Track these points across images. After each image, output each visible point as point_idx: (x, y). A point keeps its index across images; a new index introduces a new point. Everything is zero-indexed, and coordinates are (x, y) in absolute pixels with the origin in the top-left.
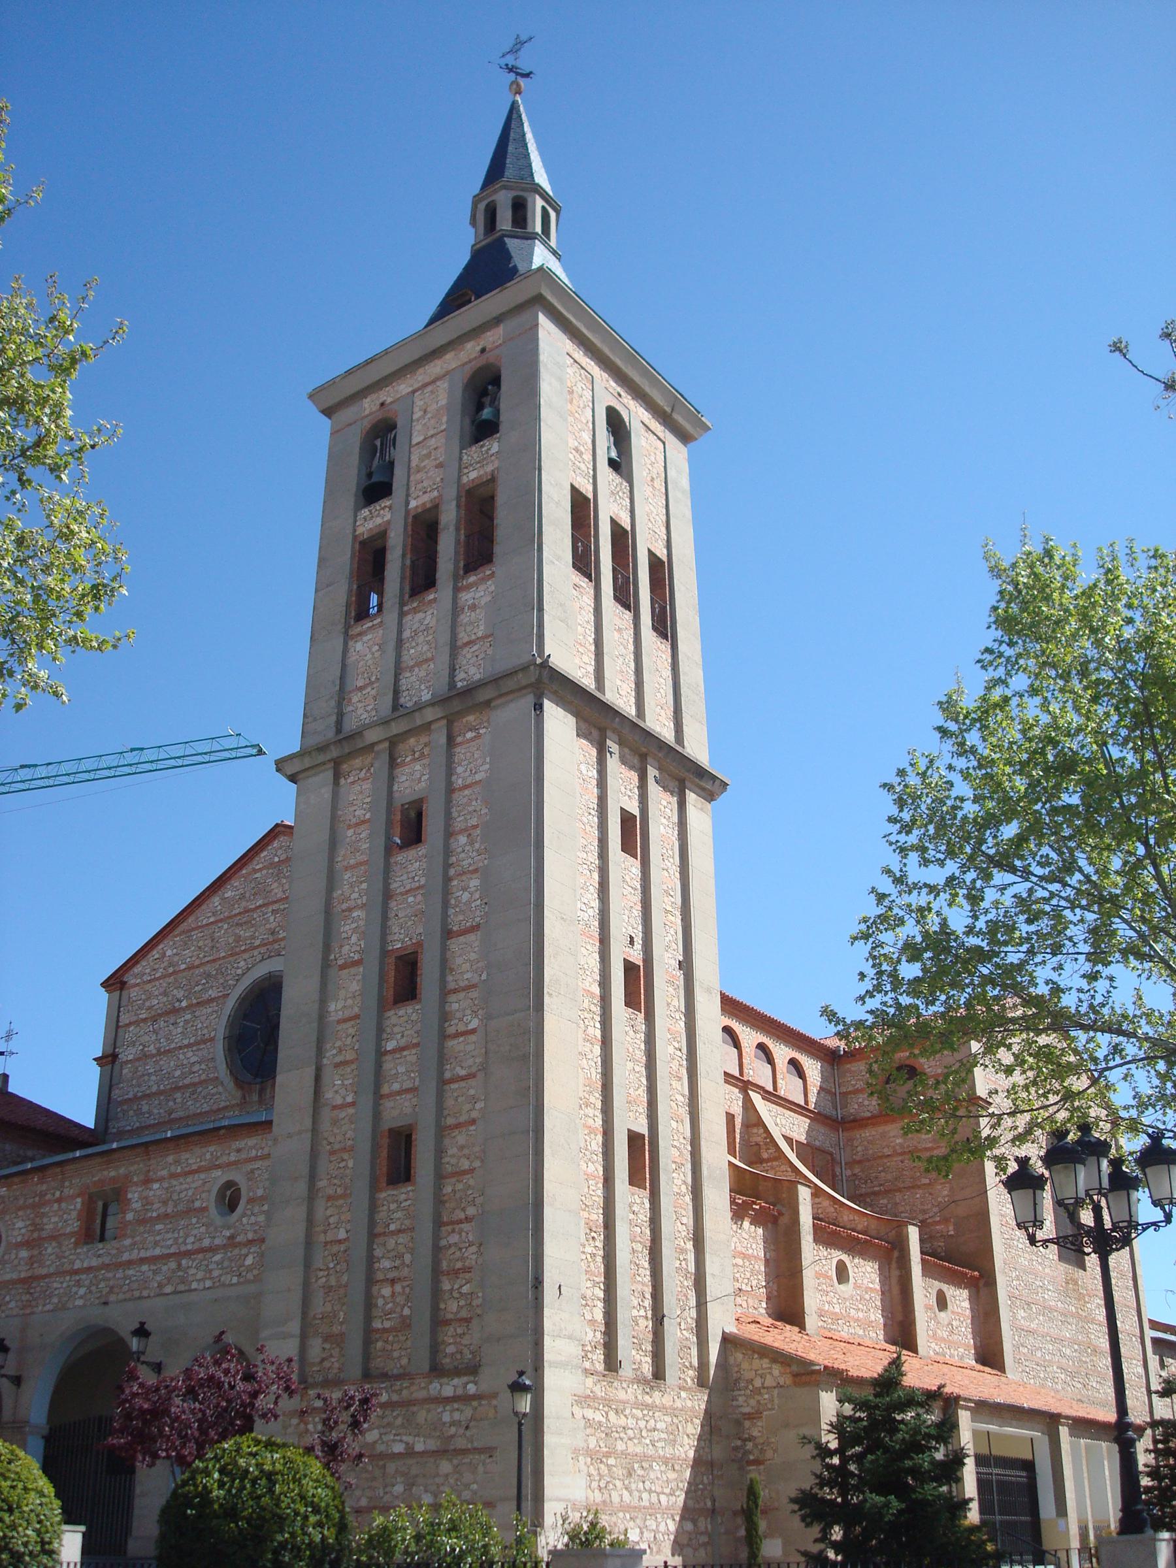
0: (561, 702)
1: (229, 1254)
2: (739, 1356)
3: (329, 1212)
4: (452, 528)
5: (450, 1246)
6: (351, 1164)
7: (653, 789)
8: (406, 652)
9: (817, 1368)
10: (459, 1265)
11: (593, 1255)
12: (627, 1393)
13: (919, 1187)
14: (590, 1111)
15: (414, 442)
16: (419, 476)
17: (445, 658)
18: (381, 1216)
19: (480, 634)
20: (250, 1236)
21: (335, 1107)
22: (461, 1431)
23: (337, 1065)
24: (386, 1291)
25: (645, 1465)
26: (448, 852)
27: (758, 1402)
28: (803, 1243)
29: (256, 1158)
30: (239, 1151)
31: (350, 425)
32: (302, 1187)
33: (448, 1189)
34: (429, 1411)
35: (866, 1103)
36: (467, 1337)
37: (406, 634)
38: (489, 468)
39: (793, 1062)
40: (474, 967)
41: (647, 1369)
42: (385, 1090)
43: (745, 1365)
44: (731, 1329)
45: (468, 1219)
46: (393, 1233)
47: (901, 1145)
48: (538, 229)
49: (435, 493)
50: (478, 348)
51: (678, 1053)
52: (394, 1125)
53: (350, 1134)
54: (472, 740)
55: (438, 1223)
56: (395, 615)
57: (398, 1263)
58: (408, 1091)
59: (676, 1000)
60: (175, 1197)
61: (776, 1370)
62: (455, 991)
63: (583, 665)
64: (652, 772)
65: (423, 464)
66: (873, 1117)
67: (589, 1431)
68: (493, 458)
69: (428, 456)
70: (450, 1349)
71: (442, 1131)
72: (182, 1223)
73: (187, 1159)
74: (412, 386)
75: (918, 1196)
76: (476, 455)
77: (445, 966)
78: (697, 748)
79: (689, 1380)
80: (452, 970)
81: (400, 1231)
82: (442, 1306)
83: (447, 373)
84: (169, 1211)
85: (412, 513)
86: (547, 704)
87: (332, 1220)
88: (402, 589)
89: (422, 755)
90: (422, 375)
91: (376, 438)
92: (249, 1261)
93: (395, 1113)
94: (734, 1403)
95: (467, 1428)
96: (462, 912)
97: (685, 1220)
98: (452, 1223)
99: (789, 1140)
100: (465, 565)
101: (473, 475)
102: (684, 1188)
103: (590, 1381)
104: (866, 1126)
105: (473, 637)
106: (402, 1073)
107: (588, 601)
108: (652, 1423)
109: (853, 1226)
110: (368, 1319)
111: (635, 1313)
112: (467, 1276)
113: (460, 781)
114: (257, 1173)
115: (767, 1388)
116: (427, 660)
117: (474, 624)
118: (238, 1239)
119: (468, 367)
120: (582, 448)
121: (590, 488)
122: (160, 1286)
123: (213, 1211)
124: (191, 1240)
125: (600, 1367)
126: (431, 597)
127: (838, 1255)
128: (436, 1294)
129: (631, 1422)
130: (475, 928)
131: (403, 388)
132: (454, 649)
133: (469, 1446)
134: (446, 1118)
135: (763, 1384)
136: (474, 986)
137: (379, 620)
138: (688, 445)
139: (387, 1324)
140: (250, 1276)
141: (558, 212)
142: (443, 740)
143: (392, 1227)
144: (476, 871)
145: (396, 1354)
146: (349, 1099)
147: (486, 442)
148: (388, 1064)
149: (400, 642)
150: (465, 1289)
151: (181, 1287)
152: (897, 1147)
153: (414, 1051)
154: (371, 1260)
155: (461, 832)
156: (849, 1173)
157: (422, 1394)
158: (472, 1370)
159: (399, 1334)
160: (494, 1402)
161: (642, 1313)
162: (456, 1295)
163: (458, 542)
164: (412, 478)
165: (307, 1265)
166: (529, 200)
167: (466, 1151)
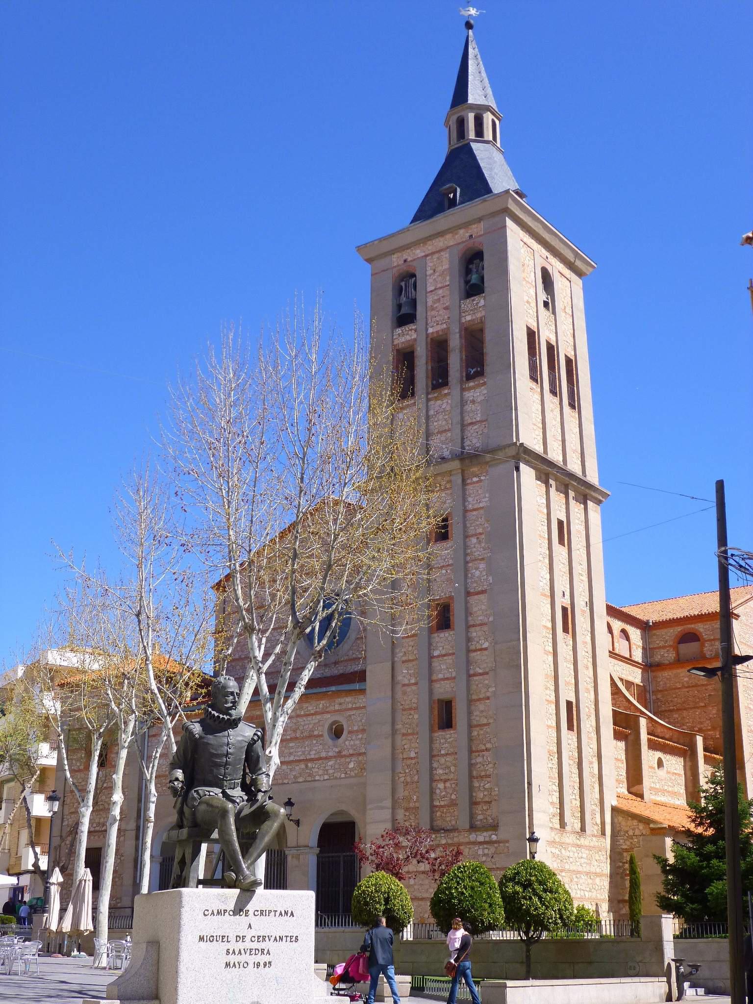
0: (527, 463)
1: (338, 761)
2: (620, 819)
3: (403, 743)
4: (457, 351)
5: (477, 764)
6: (416, 716)
7: (572, 502)
8: (432, 424)
9: (665, 826)
10: (483, 774)
11: (552, 768)
12: (570, 839)
13: (698, 708)
14: (548, 692)
15: (429, 289)
16: (433, 313)
17: (458, 430)
18: (436, 745)
19: (478, 419)
20: (351, 752)
21: (404, 685)
22: (489, 859)
23: (403, 662)
24: (441, 785)
25: (578, 876)
26: (466, 547)
27: (631, 843)
28: (642, 750)
29: (351, 709)
30: (340, 704)
31: (384, 271)
32: (387, 729)
33: (475, 733)
34: (470, 848)
35: (666, 655)
36: (489, 811)
37: (431, 412)
38: (479, 315)
39: (623, 631)
40: (485, 613)
41: (578, 826)
42: (434, 677)
43: (623, 823)
44: (615, 803)
45: (487, 750)
46: (443, 755)
47: (687, 682)
48: (491, 138)
49: (445, 326)
50: (467, 235)
51: (587, 654)
52: (442, 697)
53: (414, 700)
54: (477, 482)
55: (471, 751)
56: (424, 400)
57: (447, 771)
58: (447, 679)
59: (585, 624)
60: (301, 728)
61: (641, 826)
62: (474, 626)
63: (536, 437)
64: (571, 494)
65: (435, 306)
66: (670, 664)
67: (554, 859)
68: (481, 309)
69: (439, 300)
70: (480, 817)
71: (470, 702)
72: (307, 743)
73: (307, 707)
74: (424, 252)
75: (697, 713)
76: (469, 305)
77: (468, 612)
78: (593, 477)
79: (595, 831)
80: (471, 614)
81: (447, 754)
82: (474, 794)
83: (447, 248)
84: (298, 735)
85: (430, 337)
86: (522, 466)
87: (405, 747)
88: (427, 385)
89: (446, 489)
90: (430, 247)
91: (402, 280)
92: (351, 765)
93: (442, 690)
94: (618, 843)
95: (492, 857)
96: (476, 582)
97: (591, 746)
98: (478, 751)
99: (621, 679)
100: (466, 375)
101: (469, 318)
102: (591, 728)
103: (553, 834)
104: (665, 669)
105: (474, 420)
106: (444, 669)
107: (537, 397)
108: (580, 854)
109: (663, 736)
110: (432, 800)
111: (571, 797)
112: (488, 779)
113: (470, 506)
114: (353, 717)
115: (636, 836)
116: (445, 431)
117: (474, 412)
118: (344, 753)
119: (461, 246)
120: (530, 300)
121: (535, 325)
122: (295, 777)
123: (326, 735)
124: (314, 752)
125: (558, 826)
126: (446, 391)
127: (659, 754)
128: (471, 789)
129: (571, 854)
130: (483, 592)
131: (419, 252)
132: (463, 426)
133: (494, 867)
134: (471, 695)
135: (634, 833)
136: (485, 624)
137: (413, 401)
138: (582, 278)
139: (442, 803)
140: (353, 774)
141: (499, 120)
142: (460, 481)
143: (443, 752)
144: (483, 559)
145: (448, 819)
146: (413, 681)
147: (476, 298)
148: (436, 663)
149: (428, 417)
150: (487, 786)
151: (309, 779)
152: (685, 683)
153: (450, 657)
154: (432, 769)
155: (472, 536)
156: (654, 697)
157: (467, 840)
158: (494, 827)
159: (450, 808)
160: (507, 845)
161: (574, 797)
162: (481, 789)
163: (461, 359)
164: (429, 314)
165: (393, 770)
166: (484, 115)
167: (484, 714)
